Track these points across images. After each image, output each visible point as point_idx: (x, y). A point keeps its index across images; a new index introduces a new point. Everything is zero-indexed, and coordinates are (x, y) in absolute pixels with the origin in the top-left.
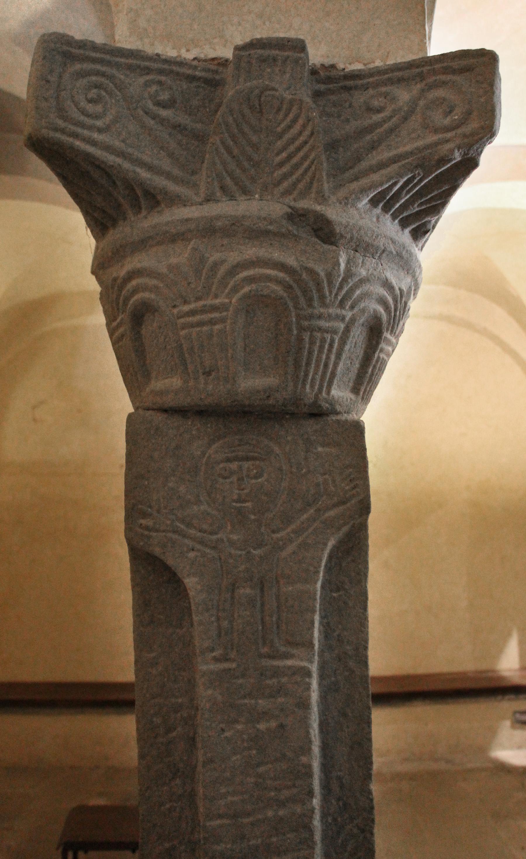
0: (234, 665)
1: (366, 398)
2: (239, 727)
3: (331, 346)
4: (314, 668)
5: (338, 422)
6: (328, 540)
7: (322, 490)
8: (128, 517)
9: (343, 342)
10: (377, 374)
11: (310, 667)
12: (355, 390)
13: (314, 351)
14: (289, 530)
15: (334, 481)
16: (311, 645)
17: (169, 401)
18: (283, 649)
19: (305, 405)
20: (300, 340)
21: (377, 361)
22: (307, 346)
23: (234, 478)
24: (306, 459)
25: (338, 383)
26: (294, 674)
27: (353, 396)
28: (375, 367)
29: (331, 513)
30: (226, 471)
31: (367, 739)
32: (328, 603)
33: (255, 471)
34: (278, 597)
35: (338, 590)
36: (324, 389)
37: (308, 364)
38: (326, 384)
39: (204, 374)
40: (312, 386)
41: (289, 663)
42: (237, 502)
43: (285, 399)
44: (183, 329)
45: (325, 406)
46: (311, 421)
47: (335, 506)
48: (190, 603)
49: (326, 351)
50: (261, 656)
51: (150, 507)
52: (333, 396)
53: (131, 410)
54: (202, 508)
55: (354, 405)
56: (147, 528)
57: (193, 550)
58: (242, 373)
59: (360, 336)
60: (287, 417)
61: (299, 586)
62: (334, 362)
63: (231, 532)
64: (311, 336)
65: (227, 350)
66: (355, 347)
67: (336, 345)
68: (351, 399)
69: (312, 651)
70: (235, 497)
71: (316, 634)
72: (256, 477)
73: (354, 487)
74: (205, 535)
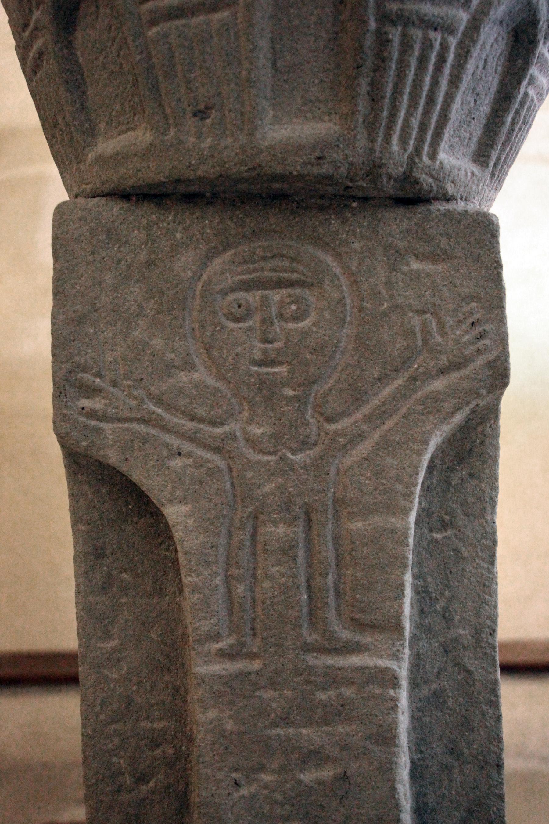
0: (257, 665)
1: (497, 175)
2: (266, 778)
3: (442, 59)
4: (403, 672)
5: (449, 214)
6: (431, 433)
7: (420, 342)
8: (59, 393)
9: (464, 53)
10: (520, 129)
11: (395, 667)
12: (481, 156)
13: (408, 66)
14: (358, 415)
15: (441, 325)
16: (399, 627)
17: (132, 174)
18: (345, 635)
19: (390, 177)
20: (382, 41)
21: (522, 104)
22: (396, 55)
23: (254, 322)
24: (388, 283)
25: (450, 140)
26: (367, 682)
27: (475, 168)
28: (517, 112)
29: (438, 384)
30: (239, 307)
31: (495, 795)
32: (427, 549)
33: (294, 307)
34: (336, 539)
35: (444, 526)
36: (426, 148)
37: (397, 92)
38: (429, 138)
39: (195, 115)
40: (403, 141)
41: (355, 660)
42: (260, 366)
43: (352, 164)
44: (153, 23)
45: (426, 180)
46: (401, 211)
47: (443, 371)
48: (176, 551)
49: (431, 67)
50: (308, 648)
51: (98, 375)
52: (441, 163)
53: (64, 196)
54: (196, 376)
55: (478, 185)
56: (92, 414)
57: (179, 454)
58: (268, 112)
59: (495, 46)
60: (354, 205)
61: (378, 520)
62: (447, 93)
63: (250, 421)
64: (404, 35)
65: (239, 63)
66: (484, 68)
67: (451, 57)
68: (473, 173)
69: (399, 640)
70: (258, 355)
71: (407, 610)
72: (297, 318)
73: (481, 337)
74: (201, 426)
